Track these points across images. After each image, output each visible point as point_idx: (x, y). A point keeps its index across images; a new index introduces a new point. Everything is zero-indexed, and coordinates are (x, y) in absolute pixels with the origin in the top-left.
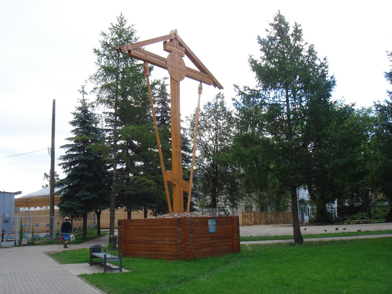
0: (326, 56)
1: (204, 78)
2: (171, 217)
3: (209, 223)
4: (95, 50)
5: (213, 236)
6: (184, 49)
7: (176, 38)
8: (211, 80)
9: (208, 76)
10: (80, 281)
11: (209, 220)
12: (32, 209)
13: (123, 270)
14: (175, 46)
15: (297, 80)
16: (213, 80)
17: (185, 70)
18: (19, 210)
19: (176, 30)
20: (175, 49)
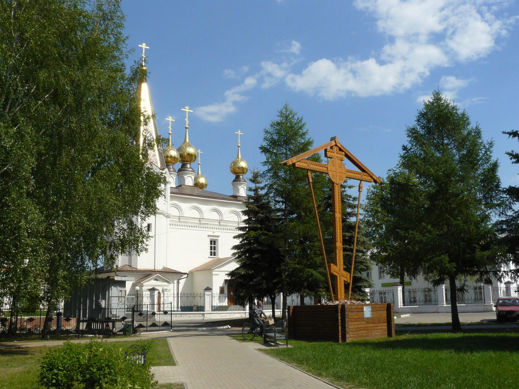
0: (504, 133)
1: (364, 177)
2: (332, 304)
3: (365, 310)
4: (286, 105)
5: (368, 320)
6: (344, 153)
7: (336, 145)
8: (370, 178)
9: (368, 175)
10: (258, 352)
11: (365, 307)
12: (339, 314)
13: (289, 346)
14: (335, 152)
15: (251, 283)
16: (374, 177)
17: (345, 172)
18: (159, 322)
19: (335, 137)
20: (335, 154)
